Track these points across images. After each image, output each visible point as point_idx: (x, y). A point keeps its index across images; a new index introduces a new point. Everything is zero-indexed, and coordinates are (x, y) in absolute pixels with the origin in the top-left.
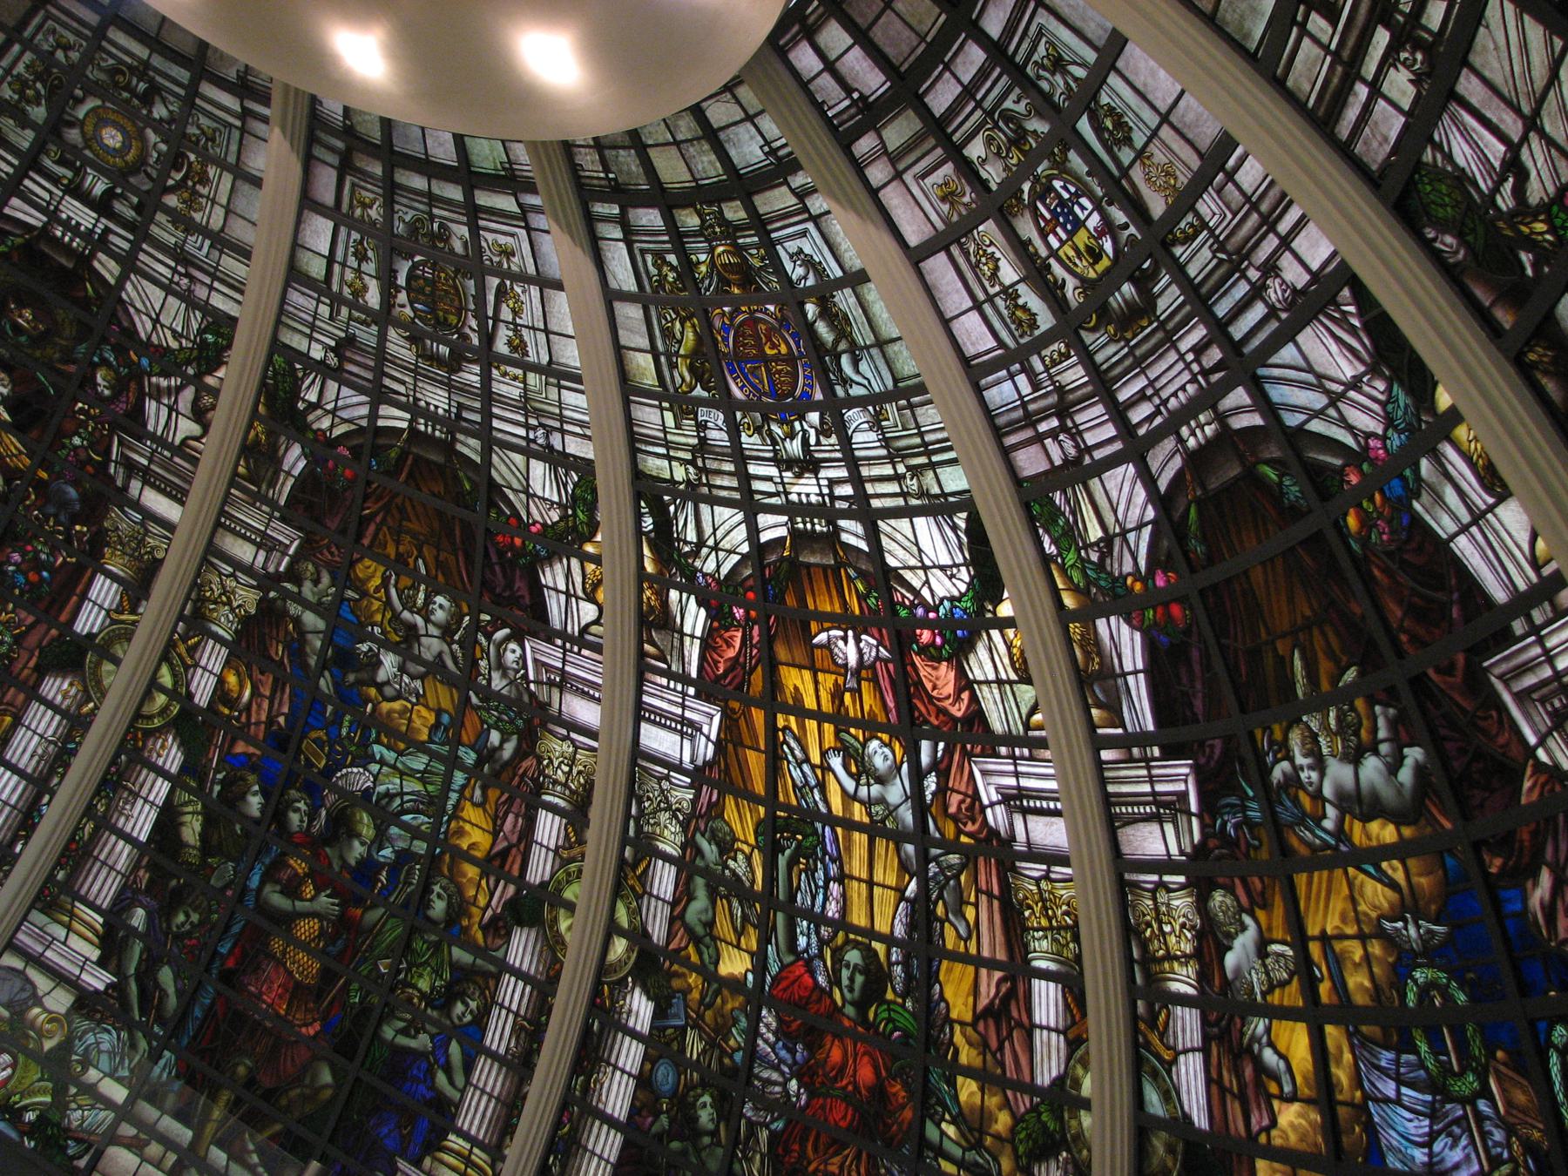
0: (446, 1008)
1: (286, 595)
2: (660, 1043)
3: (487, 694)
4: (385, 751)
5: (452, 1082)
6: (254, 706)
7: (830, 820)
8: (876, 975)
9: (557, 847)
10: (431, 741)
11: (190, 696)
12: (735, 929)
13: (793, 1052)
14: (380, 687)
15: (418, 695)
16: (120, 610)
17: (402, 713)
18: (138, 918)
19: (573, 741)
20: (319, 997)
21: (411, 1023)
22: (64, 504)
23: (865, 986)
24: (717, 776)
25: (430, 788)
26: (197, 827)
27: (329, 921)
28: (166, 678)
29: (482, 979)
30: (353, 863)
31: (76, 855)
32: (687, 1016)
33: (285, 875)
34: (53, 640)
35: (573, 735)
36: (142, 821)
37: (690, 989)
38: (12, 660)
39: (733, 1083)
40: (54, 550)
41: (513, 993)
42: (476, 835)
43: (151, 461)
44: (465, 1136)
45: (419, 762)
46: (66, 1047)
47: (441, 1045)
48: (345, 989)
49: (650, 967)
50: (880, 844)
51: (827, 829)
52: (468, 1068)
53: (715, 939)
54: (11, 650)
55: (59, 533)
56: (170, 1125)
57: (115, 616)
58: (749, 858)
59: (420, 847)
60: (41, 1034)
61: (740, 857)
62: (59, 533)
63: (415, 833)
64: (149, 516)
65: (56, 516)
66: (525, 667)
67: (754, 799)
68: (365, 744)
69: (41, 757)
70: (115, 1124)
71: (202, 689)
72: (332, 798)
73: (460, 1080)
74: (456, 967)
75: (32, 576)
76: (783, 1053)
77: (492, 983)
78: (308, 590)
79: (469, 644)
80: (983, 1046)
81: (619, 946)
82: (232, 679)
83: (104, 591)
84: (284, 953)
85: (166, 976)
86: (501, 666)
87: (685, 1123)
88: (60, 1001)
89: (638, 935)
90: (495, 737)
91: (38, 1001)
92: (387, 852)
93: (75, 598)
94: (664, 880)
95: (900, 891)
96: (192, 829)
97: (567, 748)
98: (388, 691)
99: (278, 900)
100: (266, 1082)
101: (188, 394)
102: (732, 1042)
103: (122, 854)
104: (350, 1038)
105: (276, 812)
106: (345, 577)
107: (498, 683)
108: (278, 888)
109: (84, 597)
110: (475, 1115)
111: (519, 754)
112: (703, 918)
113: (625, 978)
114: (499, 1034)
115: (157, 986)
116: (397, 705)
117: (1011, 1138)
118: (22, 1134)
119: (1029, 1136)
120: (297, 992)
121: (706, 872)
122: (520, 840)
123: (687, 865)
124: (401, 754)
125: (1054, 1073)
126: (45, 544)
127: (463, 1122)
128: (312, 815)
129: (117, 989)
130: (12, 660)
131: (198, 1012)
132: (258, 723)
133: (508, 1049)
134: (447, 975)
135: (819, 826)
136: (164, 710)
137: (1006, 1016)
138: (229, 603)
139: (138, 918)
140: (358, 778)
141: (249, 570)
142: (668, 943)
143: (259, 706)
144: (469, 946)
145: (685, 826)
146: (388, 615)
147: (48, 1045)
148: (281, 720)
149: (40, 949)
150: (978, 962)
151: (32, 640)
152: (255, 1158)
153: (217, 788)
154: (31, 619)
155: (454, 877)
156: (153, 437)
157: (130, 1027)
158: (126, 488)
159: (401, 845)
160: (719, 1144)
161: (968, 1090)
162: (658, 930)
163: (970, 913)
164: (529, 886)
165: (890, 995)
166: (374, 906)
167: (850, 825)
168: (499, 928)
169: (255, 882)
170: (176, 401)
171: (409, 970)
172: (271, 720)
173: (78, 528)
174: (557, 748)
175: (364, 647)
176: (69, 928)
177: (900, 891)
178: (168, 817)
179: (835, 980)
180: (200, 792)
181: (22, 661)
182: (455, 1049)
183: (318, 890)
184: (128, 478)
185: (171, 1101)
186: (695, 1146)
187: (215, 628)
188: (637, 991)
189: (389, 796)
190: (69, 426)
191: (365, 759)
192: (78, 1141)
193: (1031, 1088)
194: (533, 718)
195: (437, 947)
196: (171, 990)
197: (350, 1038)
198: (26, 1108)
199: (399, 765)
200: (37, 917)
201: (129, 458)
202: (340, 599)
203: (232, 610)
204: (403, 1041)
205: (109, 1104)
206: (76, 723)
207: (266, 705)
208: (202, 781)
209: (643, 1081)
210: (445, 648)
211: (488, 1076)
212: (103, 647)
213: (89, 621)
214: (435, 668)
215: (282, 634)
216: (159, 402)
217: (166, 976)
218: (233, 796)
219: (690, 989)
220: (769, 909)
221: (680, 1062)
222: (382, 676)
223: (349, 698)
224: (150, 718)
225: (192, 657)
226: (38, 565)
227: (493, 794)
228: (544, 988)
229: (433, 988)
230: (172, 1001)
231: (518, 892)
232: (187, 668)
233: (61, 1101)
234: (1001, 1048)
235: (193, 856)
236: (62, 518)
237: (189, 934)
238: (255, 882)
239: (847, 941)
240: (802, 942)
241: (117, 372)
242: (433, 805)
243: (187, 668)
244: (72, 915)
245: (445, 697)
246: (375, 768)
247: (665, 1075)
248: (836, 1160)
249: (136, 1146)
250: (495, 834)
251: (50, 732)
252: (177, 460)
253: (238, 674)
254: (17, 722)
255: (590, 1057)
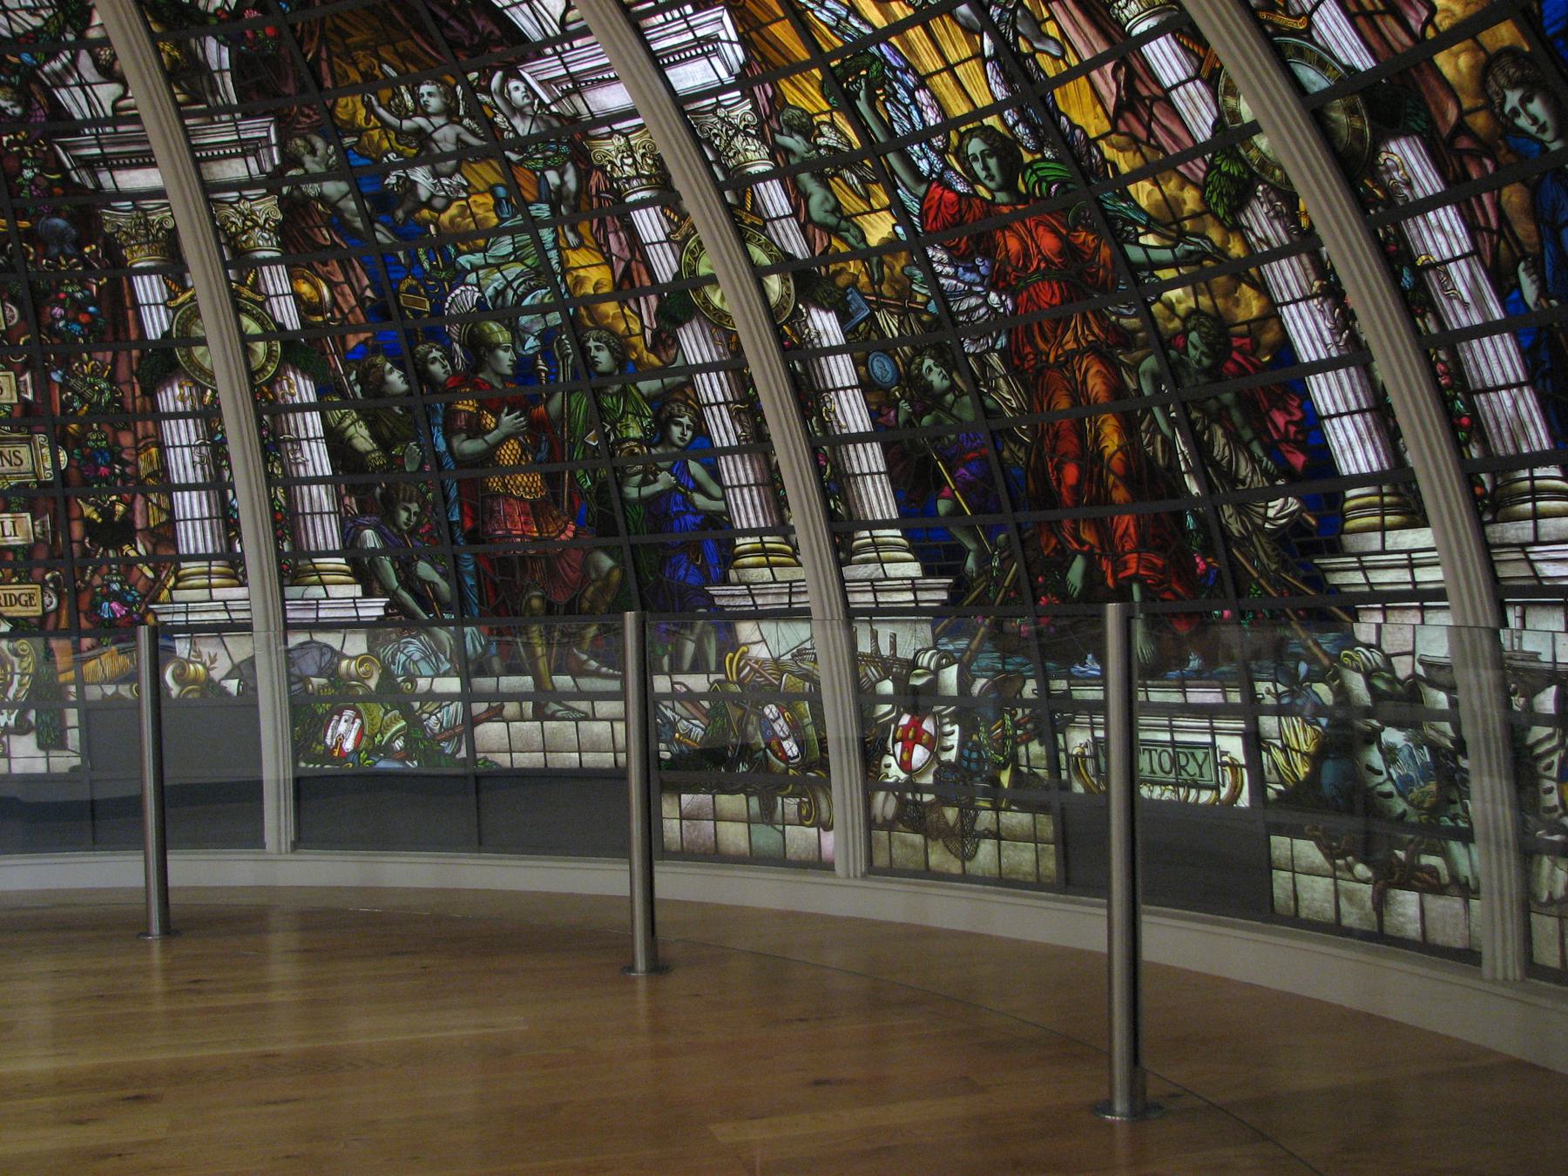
0: (665, 439)
1: (296, 182)
2: (860, 344)
3: (521, 144)
4: (470, 257)
5: (710, 497)
6: (340, 299)
7: (881, 36)
8: (1002, 147)
9: (667, 236)
10: (502, 220)
11: (281, 327)
12: (860, 197)
13: (975, 269)
14: (428, 204)
15: (465, 188)
16: (173, 297)
17: (462, 214)
18: (370, 538)
19: (619, 132)
20: (557, 504)
21: (645, 472)
22: (60, 236)
23: (1001, 166)
24: (761, 70)
25: (529, 262)
26: (365, 432)
27: (522, 434)
28: (252, 327)
29: (681, 392)
30: (509, 371)
31: (286, 522)
32: (869, 303)
33: (461, 421)
34: (139, 360)
35: (617, 127)
36: (317, 459)
37: (856, 277)
38: (120, 400)
39: (941, 332)
40: (83, 284)
41: (712, 387)
42: (594, 275)
43: (101, 146)
44: (749, 532)
45: (505, 246)
46: (387, 675)
47: (681, 471)
48: (574, 480)
49: (811, 283)
50: (936, 25)
51: (882, 47)
52: (716, 475)
53: (848, 218)
54: (113, 392)
55: (76, 265)
56: (510, 683)
57: (172, 304)
58: (832, 125)
59: (555, 318)
60: (362, 679)
61: (825, 129)
62: (76, 265)
63: (543, 309)
64: (136, 196)
65: (62, 252)
66: (536, 95)
67: (803, 67)
68: (450, 263)
69: (202, 462)
70: (467, 710)
71: (287, 314)
72: (455, 329)
73: (715, 490)
74: (650, 399)
75: (83, 318)
76: (968, 277)
77: (689, 391)
78: (311, 164)
79: (476, 111)
80: (1134, 143)
81: (774, 284)
82: (305, 288)
83: (148, 289)
84: (505, 486)
85: (424, 569)
86: (517, 110)
87: (925, 398)
88: (357, 644)
89: (784, 263)
90: (552, 177)
91: (341, 655)
92: (531, 342)
93: (130, 313)
94: (774, 197)
95: (979, 55)
96: (361, 437)
97: (619, 141)
98: (438, 203)
99: (470, 446)
100: (561, 598)
101: (85, 60)
102: (920, 299)
103: (321, 496)
104: (603, 517)
105: (419, 374)
106: (334, 130)
107: (523, 127)
108: (463, 436)
109: (136, 306)
110: (747, 511)
111: (583, 177)
112: (828, 207)
113: (796, 306)
114: (723, 429)
115: (424, 582)
116: (453, 210)
117: (1207, 208)
118: (402, 760)
119: (1220, 195)
120: (537, 510)
121: (806, 165)
122: (633, 255)
123: (785, 171)
124: (485, 250)
125: (1210, 122)
126: (72, 283)
127: (741, 522)
128: (449, 356)
129: (394, 605)
130: (120, 400)
131: (470, 581)
132: (352, 310)
133: (738, 437)
134: (648, 411)
135: (873, 49)
136: (270, 354)
137: (1139, 99)
138: (256, 224)
139: (370, 538)
140: (464, 297)
141: (251, 183)
142: (813, 252)
143: (343, 295)
144: (653, 373)
145: (761, 136)
146: (392, 136)
147: (373, 683)
148: (369, 293)
149: (312, 615)
150: (1084, 69)
151: (123, 372)
152: (594, 664)
153: (358, 389)
154: (109, 355)
155: (600, 324)
156: (86, 123)
157: (425, 627)
158: (99, 186)
159: (538, 327)
160: (962, 394)
161: (1143, 193)
162: (797, 247)
163: (1051, 29)
164: (666, 286)
165: (1027, 158)
166: (550, 396)
167: (898, 28)
168: (664, 340)
169: (441, 446)
170: (80, 75)
171: (614, 429)
172: (361, 300)
173: (87, 250)
174: (610, 148)
175: (392, 180)
176: (323, 584)
177: (979, 55)
178: (336, 441)
179: (973, 180)
180: (347, 401)
181: (128, 393)
182: (694, 467)
183: (497, 414)
184: (94, 176)
185: (496, 664)
186: (943, 409)
187: (260, 255)
188: (813, 311)
189: (500, 293)
190: (11, 164)
191: (459, 277)
192: (449, 739)
193: (1199, 149)
194: (573, 136)
195: (624, 393)
196: (436, 578)
197: (603, 517)
198: (391, 740)
199: (490, 261)
200: (292, 592)
201: (80, 157)
202: (343, 152)
203: (263, 228)
204: (646, 491)
205: (450, 697)
206: (208, 416)
207: (347, 290)
208: (342, 393)
209: (866, 385)
210: (459, 129)
211: (737, 471)
212: (184, 336)
213: (155, 324)
214: (463, 153)
215: (317, 219)
216: (66, 86)
217: (424, 569)
218: (374, 386)
219: (856, 277)
220: (877, 158)
221: (888, 348)
222: (424, 194)
223: (410, 233)
224: (263, 369)
225: (260, 293)
226: (80, 306)
227: (584, 228)
228: (734, 365)
229: (644, 430)
230: (444, 586)
231: (660, 297)
232: (261, 305)
233: (414, 721)
234: (1151, 134)
235: (377, 458)
236: (69, 251)
237: (419, 522)
238: (441, 446)
239: (962, 136)
240: (924, 166)
241: (11, 85)
242: (542, 274)
243: (261, 305)
244: (318, 572)
245: (488, 173)
246: (472, 278)
247: (881, 368)
248: (1069, 336)
249: (495, 715)
250: (608, 262)
251: (193, 438)
252: (121, 129)
253: (307, 280)
254: (162, 448)
255: (809, 396)
